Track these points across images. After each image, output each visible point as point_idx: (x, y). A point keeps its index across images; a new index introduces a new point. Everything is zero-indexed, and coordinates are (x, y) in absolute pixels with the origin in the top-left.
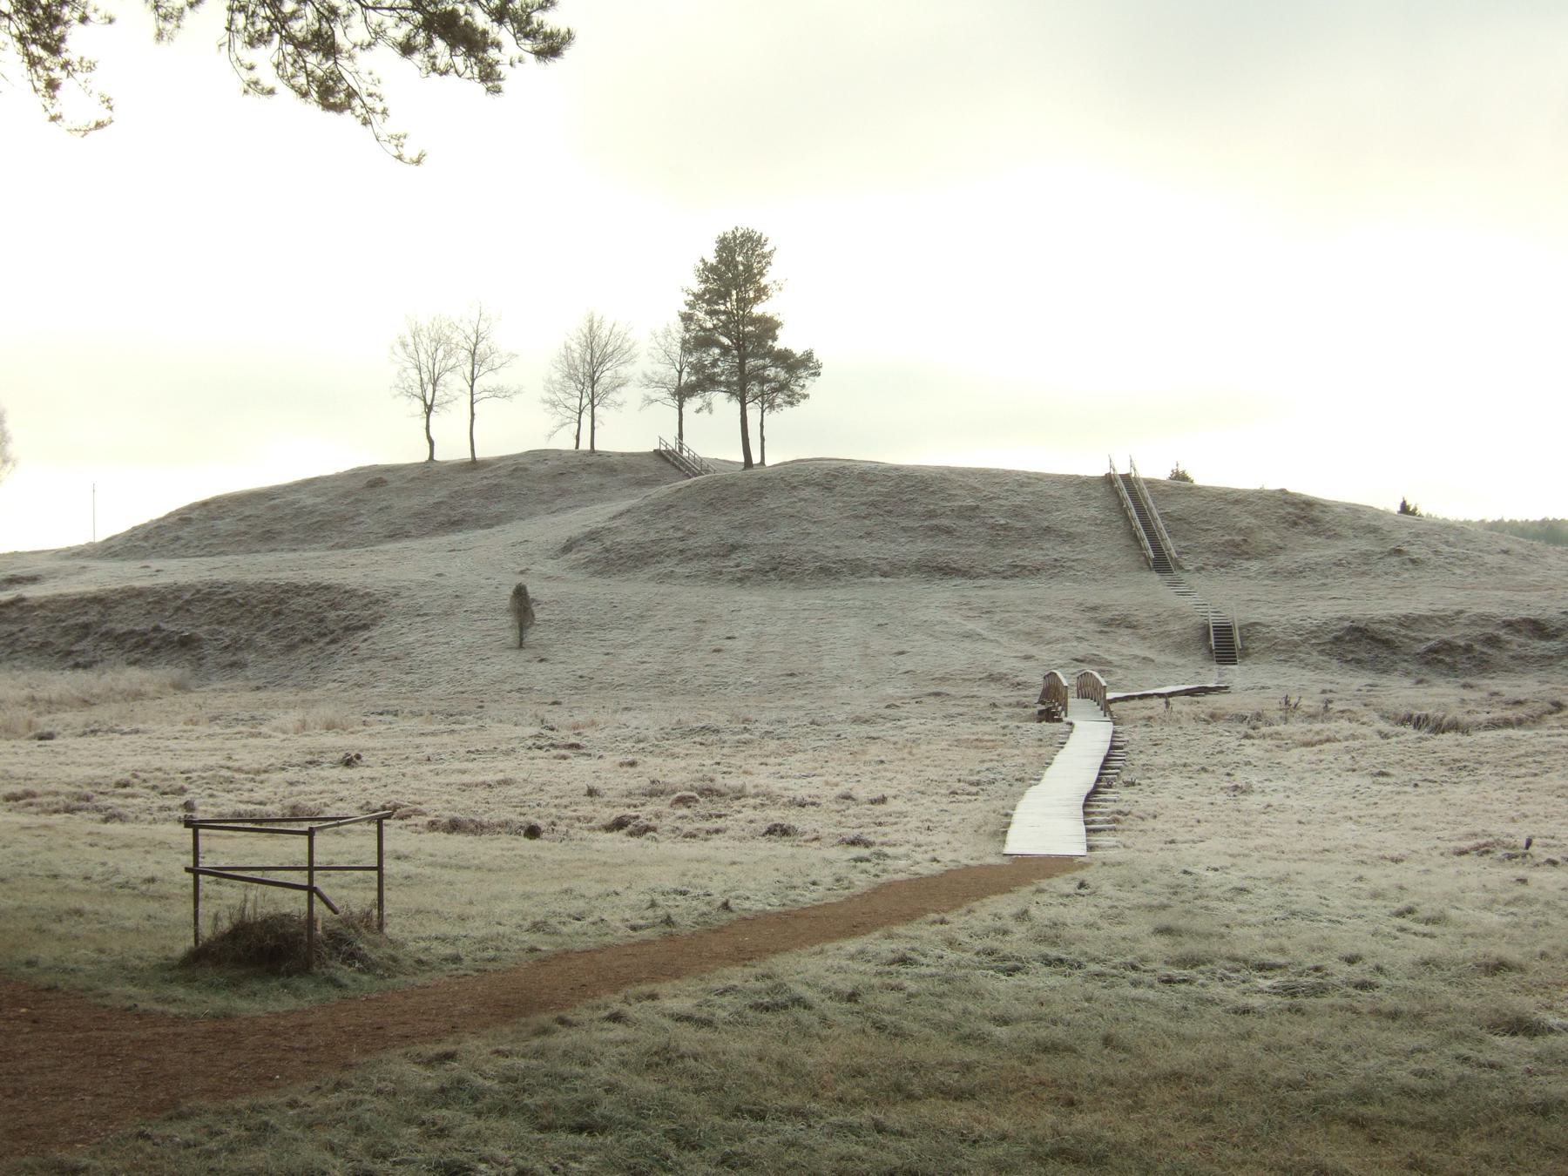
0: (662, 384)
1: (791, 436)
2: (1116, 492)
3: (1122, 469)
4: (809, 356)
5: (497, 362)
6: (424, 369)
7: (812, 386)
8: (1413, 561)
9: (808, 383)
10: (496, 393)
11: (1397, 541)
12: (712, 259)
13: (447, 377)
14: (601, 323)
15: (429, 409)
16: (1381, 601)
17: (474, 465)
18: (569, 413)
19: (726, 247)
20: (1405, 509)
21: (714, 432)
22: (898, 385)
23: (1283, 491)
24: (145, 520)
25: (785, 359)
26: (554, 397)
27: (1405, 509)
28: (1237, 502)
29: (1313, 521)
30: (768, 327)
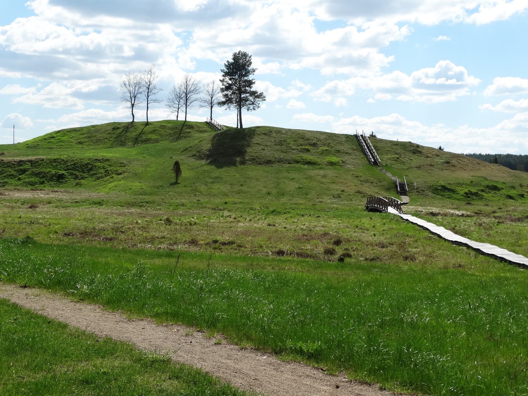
0: (205, 101)
1: (251, 119)
2: (358, 140)
3: (360, 133)
4: (261, 94)
5: (156, 91)
6: (132, 93)
7: (263, 105)
8: (453, 166)
9: (261, 103)
10: (155, 101)
11: (451, 161)
12: (231, 61)
13: (139, 96)
14: (190, 80)
15: (133, 105)
16: (445, 177)
17: (147, 124)
18: (175, 109)
19: (236, 57)
20: (440, 148)
21: (226, 118)
22: (284, 105)
23: (410, 142)
24: (455, 152)
25: (253, 93)
26: (170, 104)
27: (440, 148)
28: (397, 145)
29: (420, 152)
30: (250, 83)
